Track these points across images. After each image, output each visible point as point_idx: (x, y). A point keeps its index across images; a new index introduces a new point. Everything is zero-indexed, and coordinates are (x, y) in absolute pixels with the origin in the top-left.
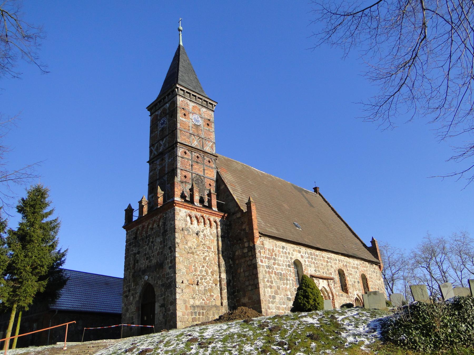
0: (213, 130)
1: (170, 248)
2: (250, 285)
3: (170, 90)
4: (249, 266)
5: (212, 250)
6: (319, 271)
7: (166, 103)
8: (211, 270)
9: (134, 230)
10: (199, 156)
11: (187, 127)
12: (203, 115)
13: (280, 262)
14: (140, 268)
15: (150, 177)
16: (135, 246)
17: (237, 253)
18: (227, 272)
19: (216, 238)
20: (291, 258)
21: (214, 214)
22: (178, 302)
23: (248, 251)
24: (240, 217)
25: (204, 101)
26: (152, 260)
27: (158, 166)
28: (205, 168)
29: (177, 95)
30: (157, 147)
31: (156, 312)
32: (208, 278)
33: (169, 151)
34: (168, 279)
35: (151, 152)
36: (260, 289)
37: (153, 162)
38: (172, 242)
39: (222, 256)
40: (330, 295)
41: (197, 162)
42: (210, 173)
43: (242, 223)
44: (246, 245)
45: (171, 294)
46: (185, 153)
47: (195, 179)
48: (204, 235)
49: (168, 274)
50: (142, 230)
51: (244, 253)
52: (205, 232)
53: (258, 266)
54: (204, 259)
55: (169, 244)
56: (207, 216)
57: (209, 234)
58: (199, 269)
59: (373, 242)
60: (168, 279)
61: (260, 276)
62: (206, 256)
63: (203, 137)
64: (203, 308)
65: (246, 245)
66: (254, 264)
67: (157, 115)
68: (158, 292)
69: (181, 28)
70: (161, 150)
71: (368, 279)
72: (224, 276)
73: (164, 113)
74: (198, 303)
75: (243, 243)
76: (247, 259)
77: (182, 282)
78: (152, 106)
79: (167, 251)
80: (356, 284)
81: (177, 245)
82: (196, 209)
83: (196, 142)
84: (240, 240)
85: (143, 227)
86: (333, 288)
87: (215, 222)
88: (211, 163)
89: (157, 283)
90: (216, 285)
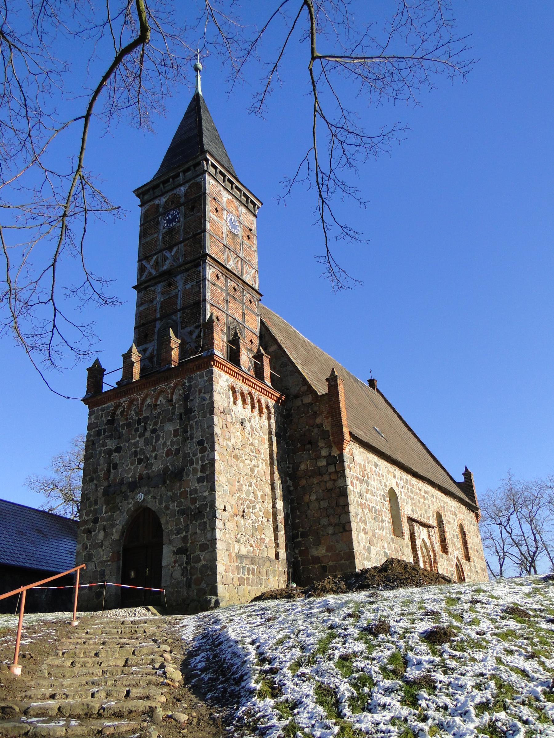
0: (256, 249)
1: (200, 443)
2: (330, 524)
3: (191, 163)
4: (330, 490)
5: (262, 456)
6: (417, 513)
7: (180, 185)
8: (261, 493)
9: (108, 407)
10: (237, 287)
11: (220, 233)
12: (242, 218)
13: (373, 489)
14: (122, 480)
15: (139, 316)
16: (111, 437)
17: (303, 467)
18: (286, 499)
19: (267, 437)
20: (386, 486)
21: (263, 391)
22: (220, 545)
23: (328, 464)
24: (311, 404)
25: (245, 195)
26: (152, 464)
27: (159, 296)
28: (246, 312)
29: (205, 172)
30: (157, 262)
31: (164, 563)
32: (257, 505)
33: (187, 270)
34: (194, 501)
35: (142, 270)
36: (353, 533)
37: (146, 288)
38: (204, 431)
39: (278, 469)
40: (431, 553)
41: (234, 298)
42: (251, 321)
43: (315, 415)
44: (324, 453)
45: (204, 529)
46: (218, 278)
47: (231, 327)
48: (251, 427)
49: (196, 491)
50: (129, 408)
51: (319, 468)
52: (252, 421)
53: (348, 492)
54: (252, 471)
55: (199, 436)
56: (257, 393)
57: (258, 426)
58: (246, 488)
59: (467, 474)
60: (194, 501)
61: (352, 509)
62: (255, 466)
63: (241, 256)
64: (253, 560)
65: (324, 453)
66: (340, 488)
67: (158, 206)
68: (168, 525)
69: (200, 66)
70: (165, 268)
71: (467, 533)
72: (280, 505)
73: (175, 203)
74: (244, 550)
75: (317, 449)
76: (326, 478)
77: (225, 510)
78: (147, 187)
79: (191, 448)
80: (455, 539)
81: (216, 439)
82: (243, 378)
83: (231, 262)
84: (310, 443)
85: (131, 402)
86: (435, 543)
87: (268, 407)
88: (253, 305)
89: (167, 508)
90: (268, 521)
